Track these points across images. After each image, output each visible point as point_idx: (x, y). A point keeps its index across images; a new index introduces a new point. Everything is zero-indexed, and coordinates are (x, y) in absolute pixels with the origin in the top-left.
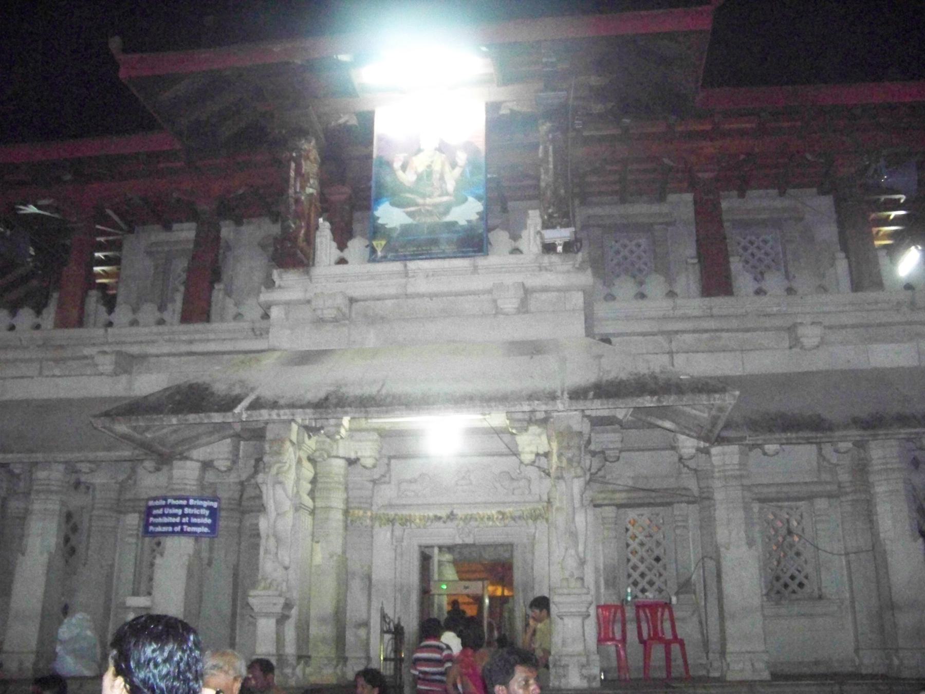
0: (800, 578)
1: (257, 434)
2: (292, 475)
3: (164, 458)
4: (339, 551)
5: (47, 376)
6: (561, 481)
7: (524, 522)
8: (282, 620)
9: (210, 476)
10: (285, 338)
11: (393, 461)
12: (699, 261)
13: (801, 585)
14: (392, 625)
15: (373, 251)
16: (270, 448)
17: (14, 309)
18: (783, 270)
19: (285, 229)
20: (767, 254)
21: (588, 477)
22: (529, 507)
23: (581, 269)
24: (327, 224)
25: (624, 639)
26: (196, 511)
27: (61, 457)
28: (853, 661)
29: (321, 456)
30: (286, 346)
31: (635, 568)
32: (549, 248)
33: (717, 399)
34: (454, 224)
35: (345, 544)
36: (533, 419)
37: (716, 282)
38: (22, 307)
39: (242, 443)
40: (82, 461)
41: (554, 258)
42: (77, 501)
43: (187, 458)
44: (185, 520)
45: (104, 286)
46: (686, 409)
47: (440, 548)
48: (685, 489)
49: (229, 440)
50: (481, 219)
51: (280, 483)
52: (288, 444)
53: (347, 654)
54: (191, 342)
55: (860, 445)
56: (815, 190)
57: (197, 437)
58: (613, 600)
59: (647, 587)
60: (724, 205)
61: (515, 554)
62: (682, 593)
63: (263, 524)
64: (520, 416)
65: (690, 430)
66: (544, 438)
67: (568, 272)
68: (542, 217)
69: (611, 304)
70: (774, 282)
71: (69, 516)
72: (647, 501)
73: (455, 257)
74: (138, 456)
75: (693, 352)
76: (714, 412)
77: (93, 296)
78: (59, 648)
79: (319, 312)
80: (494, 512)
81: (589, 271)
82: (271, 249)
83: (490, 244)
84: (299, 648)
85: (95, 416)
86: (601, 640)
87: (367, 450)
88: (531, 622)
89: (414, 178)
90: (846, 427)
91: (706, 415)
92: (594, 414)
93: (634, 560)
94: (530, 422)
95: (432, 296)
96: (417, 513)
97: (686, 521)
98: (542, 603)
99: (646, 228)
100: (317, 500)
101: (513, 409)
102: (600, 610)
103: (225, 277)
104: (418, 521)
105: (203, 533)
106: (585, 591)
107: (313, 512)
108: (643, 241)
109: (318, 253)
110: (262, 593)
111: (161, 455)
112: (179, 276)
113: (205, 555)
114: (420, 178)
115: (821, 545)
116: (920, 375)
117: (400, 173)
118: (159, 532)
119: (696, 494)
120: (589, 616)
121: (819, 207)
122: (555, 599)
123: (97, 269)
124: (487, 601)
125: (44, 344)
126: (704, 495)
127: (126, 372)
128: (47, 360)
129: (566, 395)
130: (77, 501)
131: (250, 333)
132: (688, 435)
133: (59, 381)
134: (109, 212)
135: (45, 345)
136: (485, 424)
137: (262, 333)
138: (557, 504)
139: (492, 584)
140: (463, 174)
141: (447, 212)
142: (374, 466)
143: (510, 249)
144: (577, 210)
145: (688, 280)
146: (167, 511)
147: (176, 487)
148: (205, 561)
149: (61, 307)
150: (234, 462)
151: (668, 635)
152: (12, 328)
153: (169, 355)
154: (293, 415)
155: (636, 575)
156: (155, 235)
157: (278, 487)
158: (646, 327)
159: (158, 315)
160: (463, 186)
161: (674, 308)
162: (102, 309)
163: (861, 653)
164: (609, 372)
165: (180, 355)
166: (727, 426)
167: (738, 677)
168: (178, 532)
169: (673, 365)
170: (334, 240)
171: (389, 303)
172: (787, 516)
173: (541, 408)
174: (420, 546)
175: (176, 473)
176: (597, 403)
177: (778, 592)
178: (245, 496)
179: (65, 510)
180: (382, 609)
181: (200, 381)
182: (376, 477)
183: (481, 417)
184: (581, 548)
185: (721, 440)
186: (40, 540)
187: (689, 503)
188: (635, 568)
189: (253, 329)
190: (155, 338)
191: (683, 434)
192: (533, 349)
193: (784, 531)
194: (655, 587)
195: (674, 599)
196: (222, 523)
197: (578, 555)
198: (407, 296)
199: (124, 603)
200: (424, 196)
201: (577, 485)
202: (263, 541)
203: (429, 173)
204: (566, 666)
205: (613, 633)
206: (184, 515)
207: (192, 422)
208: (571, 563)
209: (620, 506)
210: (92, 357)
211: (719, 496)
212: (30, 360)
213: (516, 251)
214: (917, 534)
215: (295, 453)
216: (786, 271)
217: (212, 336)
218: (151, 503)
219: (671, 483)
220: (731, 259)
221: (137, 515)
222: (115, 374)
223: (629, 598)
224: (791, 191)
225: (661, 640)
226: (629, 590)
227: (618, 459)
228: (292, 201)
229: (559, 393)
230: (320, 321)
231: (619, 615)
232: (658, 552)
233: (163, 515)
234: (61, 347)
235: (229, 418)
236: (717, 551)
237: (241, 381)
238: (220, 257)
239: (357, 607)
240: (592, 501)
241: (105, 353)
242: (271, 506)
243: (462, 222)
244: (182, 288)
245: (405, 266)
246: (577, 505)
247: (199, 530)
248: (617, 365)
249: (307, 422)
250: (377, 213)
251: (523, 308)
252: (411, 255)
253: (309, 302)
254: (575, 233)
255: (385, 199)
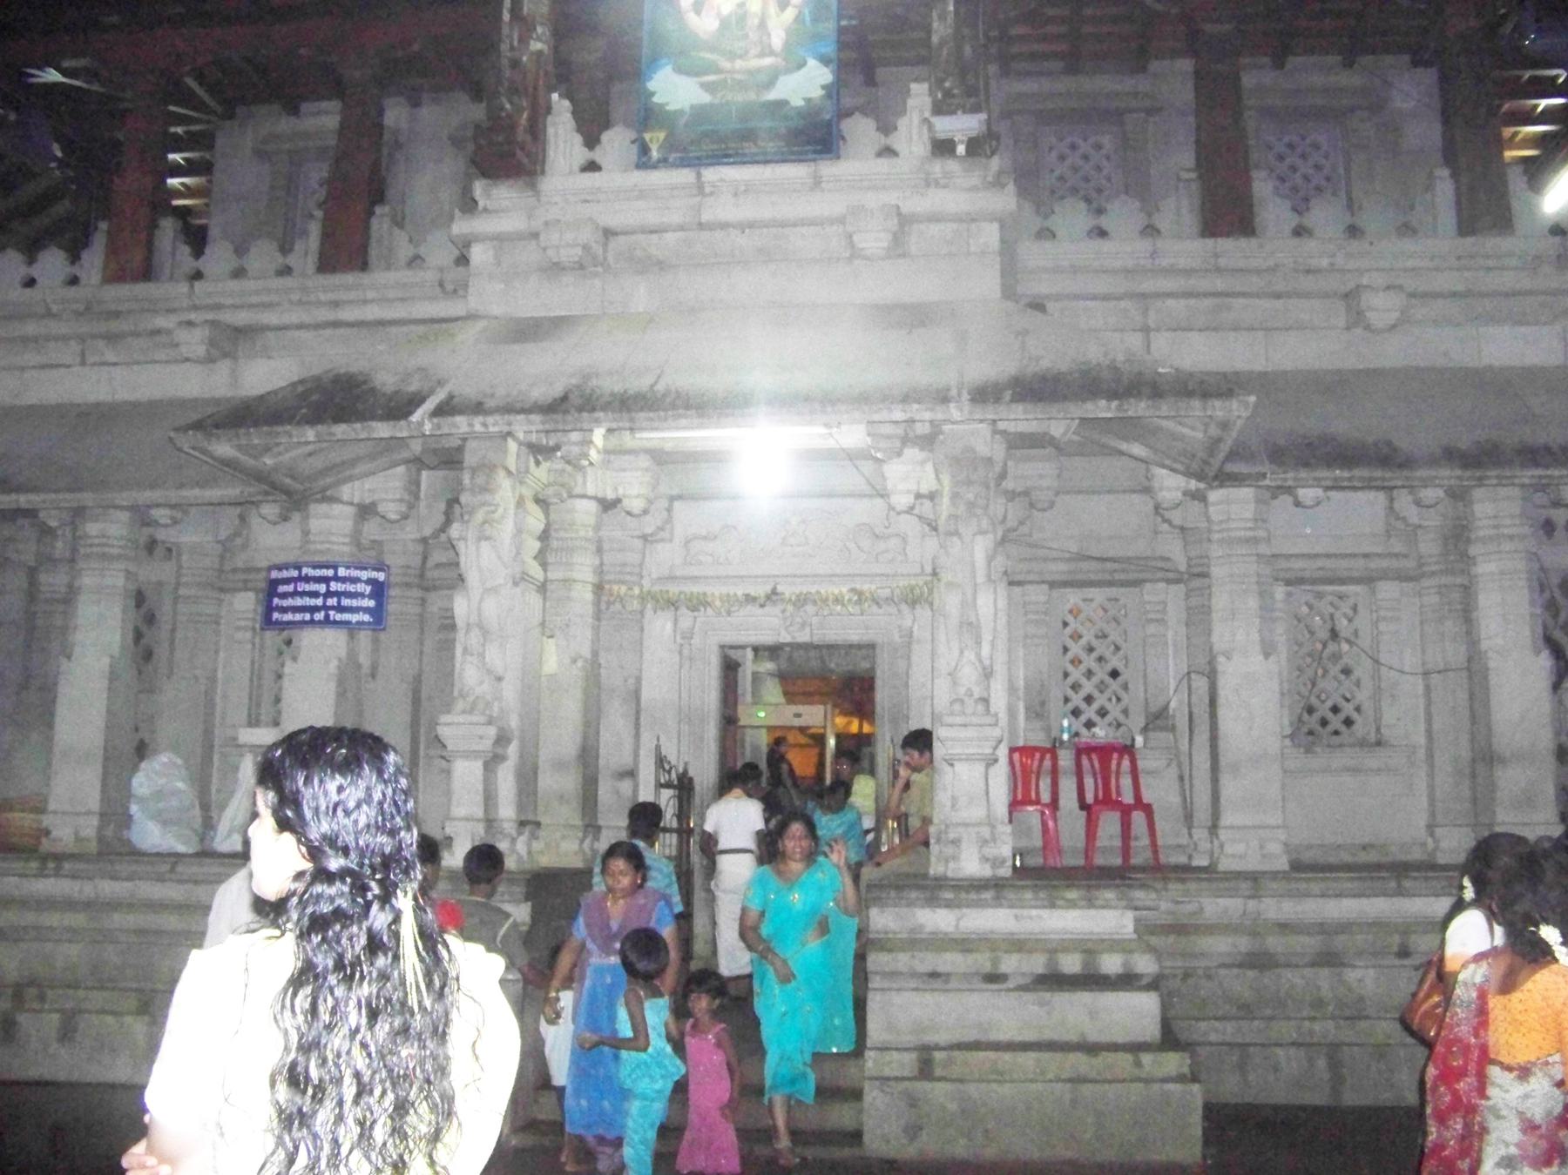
0: (1348, 709)
1: (450, 459)
2: (509, 527)
3: (295, 497)
4: (586, 652)
5: (94, 364)
6: (955, 539)
7: (893, 610)
8: (492, 763)
9: (371, 529)
10: (494, 295)
11: (677, 504)
12: (1200, 177)
13: (1348, 722)
14: (674, 776)
15: (644, 150)
16: (472, 478)
17: (32, 249)
18: (1343, 194)
19: (494, 114)
20: (1318, 167)
21: (1000, 534)
22: (903, 583)
23: (997, 184)
24: (567, 103)
25: (1054, 804)
26: (351, 588)
27: (125, 498)
28: (1424, 844)
29: (558, 495)
30: (496, 310)
31: (1075, 687)
32: (943, 148)
33: (1218, 409)
34: (782, 104)
35: (596, 639)
36: (911, 435)
37: (1227, 214)
38: (45, 247)
39: (424, 473)
40: (158, 506)
41: (952, 165)
42: (155, 572)
43: (337, 500)
44: (332, 601)
45: (184, 213)
46: (1164, 423)
47: (756, 649)
48: (1163, 559)
49: (401, 469)
50: (829, 96)
51: (487, 538)
52: (502, 473)
53: (601, 822)
54: (336, 304)
55: (1458, 495)
56: (1407, 58)
57: (353, 462)
58: (1038, 739)
59: (1096, 718)
60: (1248, 80)
61: (879, 661)
62: (1154, 730)
63: (461, 607)
64: (888, 429)
65: (1175, 460)
66: (929, 467)
67: (974, 189)
68: (931, 93)
69: (1048, 245)
70: (1325, 216)
71: (140, 598)
72: (1100, 577)
73: (784, 161)
74: (250, 495)
75: (1184, 330)
76: (1214, 431)
77: (168, 228)
78: (134, 809)
79: (550, 252)
80: (844, 590)
81: (1011, 188)
82: (471, 147)
83: (843, 138)
84: (520, 807)
85: (176, 430)
86: (1015, 805)
87: (633, 485)
88: (903, 772)
89: (716, 24)
90: (1433, 462)
91: (1200, 435)
92: (1011, 427)
93: (1076, 674)
94: (905, 440)
95: (745, 226)
96: (715, 590)
97: (1164, 611)
98: (920, 740)
99: (1113, 116)
100: (550, 568)
101: (876, 417)
102: (1016, 756)
103: (391, 193)
104: (718, 603)
105: (363, 623)
106: (989, 720)
107: (543, 588)
108: (1107, 141)
109: (551, 153)
110: (461, 719)
111: (288, 493)
112: (314, 193)
113: (364, 660)
114: (725, 23)
115: (1383, 658)
116: (1564, 382)
117: (692, 19)
118: (289, 623)
119: (1183, 568)
120: (996, 761)
121: (1411, 92)
122: (940, 733)
123: (174, 182)
124: (832, 742)
125: (87, 309)
126: (1196, 570)
127: (226, 355)
128: (94, 337)
129: (966, 396)
130: (155, 572)
131: (438, 289)
132: (1172, 470)
133: (117, 372)
134: (191, 82)
135: (88, 311)
136: (831, 443)
137: (460, 290)
138: (946, 576)
139: (845, 713)
140: (799, 19)
141: (770, 84)
142: (645, 512)
143: (877, 147)
144: (993, 83)
145: (1179, 209)
146: (303, 587)
147: (312, 547)
148: (366, 670)
149: (113, 250)
150: (411, 507)
151: (1128, 798)
152: (30, 283)
153: (300, 327)
154: (510, 424)
155: (1077, 700)
156: (273, 123)
157: (484, 544)
158: (1102, 285)
159: (280, 260)
160: (799, 38)
161: (1154, 254)
162: (185, 250)
163: (1439, 831)
164: (1038, 359)
165: (318, 326)
166: (1233, 456)
167: (1236, 866)
168: (320, 622)
169: (1149, 352)
170: (579, 130)
171: (670, 237)
172: (1332, 610)
173: (924, 415)
174: (722, 647)
175: (315, 524)
176: (1019, 410)
177: (1311, 733)
178: (430, 563)
179: (132, 587)
180: (658, 748)
181: (354, 369)
182: (649, 530)
183: (823, 430)
184: (986, 650)
185: (1224, 479)
186: (96, 637)
187: (1169, 581)
188: (1075, 687)
189: (441, 285)
190: (274, 298)
191: (1163, 466)
192: (914, 317)
193: (1323, 634)
194: (1109, 718)
195: (1139, 740)
196: (392, 607)
197: (981, 661)
198: (701, 226)
199: (235, 739)
200: (732, 56)
201: (981, 548)
202: (460, 636)
203: (741, 17)
204: (956, 842)
205: (1038, 793)
206: (329, 594)
207: (339, 437)
208: (969, 675)
209: (1053, 585)
210: (169, 332)
211: (1217, 571)
212: (65, 339)
213: (888, 152)
214: (1540, 643)
215: (513, 488)
216: (1350, 199)
217: (370, 295)
218: (275, 574)
219: (1139, 548)
220: (1255, 174)
221: (251, 595)
222: (210, 360)
223: (1065, 737)
224: (1367, 60)
225: (1117, 805)
226: (1065, 723)
227: (1052, 505)
228: (505, 62)
229: (954, 392)
230: (554, 269)
231: (1047, 763)
232: (1115, 662)
233: (295, 593)
234: (117, 315)
235: (400, 430)
236: (1212, 662)
237: (420, 369)
238: (384, 161)
239: (614, 748)
240: (1005, 573)
241: (190, 324)
242: (472, 578)
243: (797, 102)
244: (319, 214)
245: (699, 175)
246: (981, 579)
247: (354, 618)
248: (1053, 350)
249: (533, 438)
250: (652, 85)
251: (898, 247)
252: (707, 157)
253: (535, 235)
254: (989, 122)
255: (664, 61)
